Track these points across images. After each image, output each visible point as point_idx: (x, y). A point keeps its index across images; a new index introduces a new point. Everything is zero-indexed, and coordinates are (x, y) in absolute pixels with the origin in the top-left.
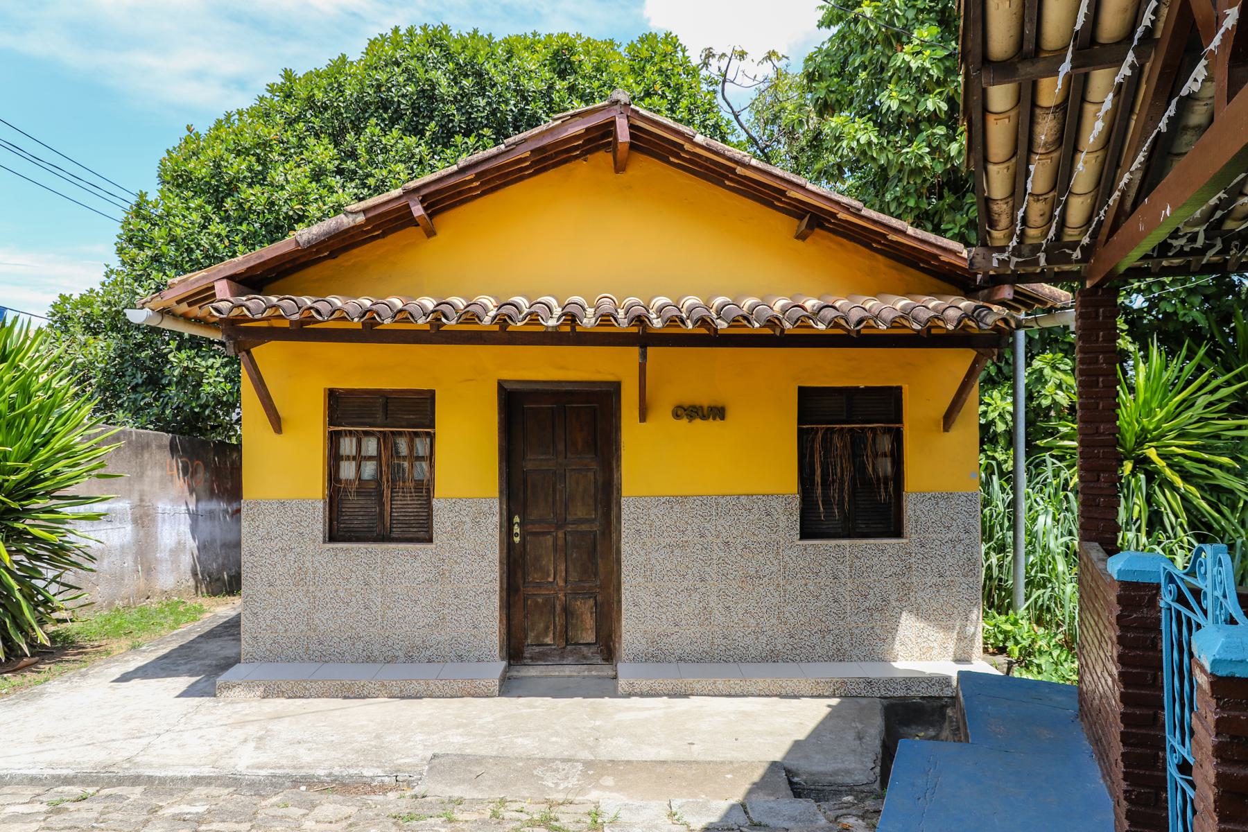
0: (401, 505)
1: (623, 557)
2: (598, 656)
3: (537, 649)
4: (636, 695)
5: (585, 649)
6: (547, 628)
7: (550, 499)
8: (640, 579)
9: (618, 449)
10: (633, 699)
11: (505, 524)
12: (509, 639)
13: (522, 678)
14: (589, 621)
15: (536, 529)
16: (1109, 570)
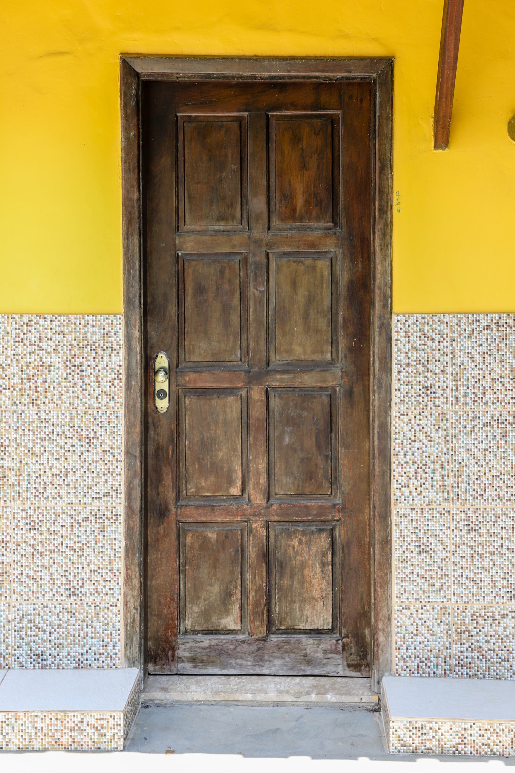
1: (395, 445)
2: (338, 659)
3: (206, 641)
4: (428, 753)
5: (309, 643)
6: (227, 595)
7: (235, 319)
8: (432, 495)
9: (386, 209)
10: (421, 762)
11: (138, 371)
12: (145, 620)
13: (173, 705)
14: (318, 582)
15: (206, 381)
16: (167, 405)
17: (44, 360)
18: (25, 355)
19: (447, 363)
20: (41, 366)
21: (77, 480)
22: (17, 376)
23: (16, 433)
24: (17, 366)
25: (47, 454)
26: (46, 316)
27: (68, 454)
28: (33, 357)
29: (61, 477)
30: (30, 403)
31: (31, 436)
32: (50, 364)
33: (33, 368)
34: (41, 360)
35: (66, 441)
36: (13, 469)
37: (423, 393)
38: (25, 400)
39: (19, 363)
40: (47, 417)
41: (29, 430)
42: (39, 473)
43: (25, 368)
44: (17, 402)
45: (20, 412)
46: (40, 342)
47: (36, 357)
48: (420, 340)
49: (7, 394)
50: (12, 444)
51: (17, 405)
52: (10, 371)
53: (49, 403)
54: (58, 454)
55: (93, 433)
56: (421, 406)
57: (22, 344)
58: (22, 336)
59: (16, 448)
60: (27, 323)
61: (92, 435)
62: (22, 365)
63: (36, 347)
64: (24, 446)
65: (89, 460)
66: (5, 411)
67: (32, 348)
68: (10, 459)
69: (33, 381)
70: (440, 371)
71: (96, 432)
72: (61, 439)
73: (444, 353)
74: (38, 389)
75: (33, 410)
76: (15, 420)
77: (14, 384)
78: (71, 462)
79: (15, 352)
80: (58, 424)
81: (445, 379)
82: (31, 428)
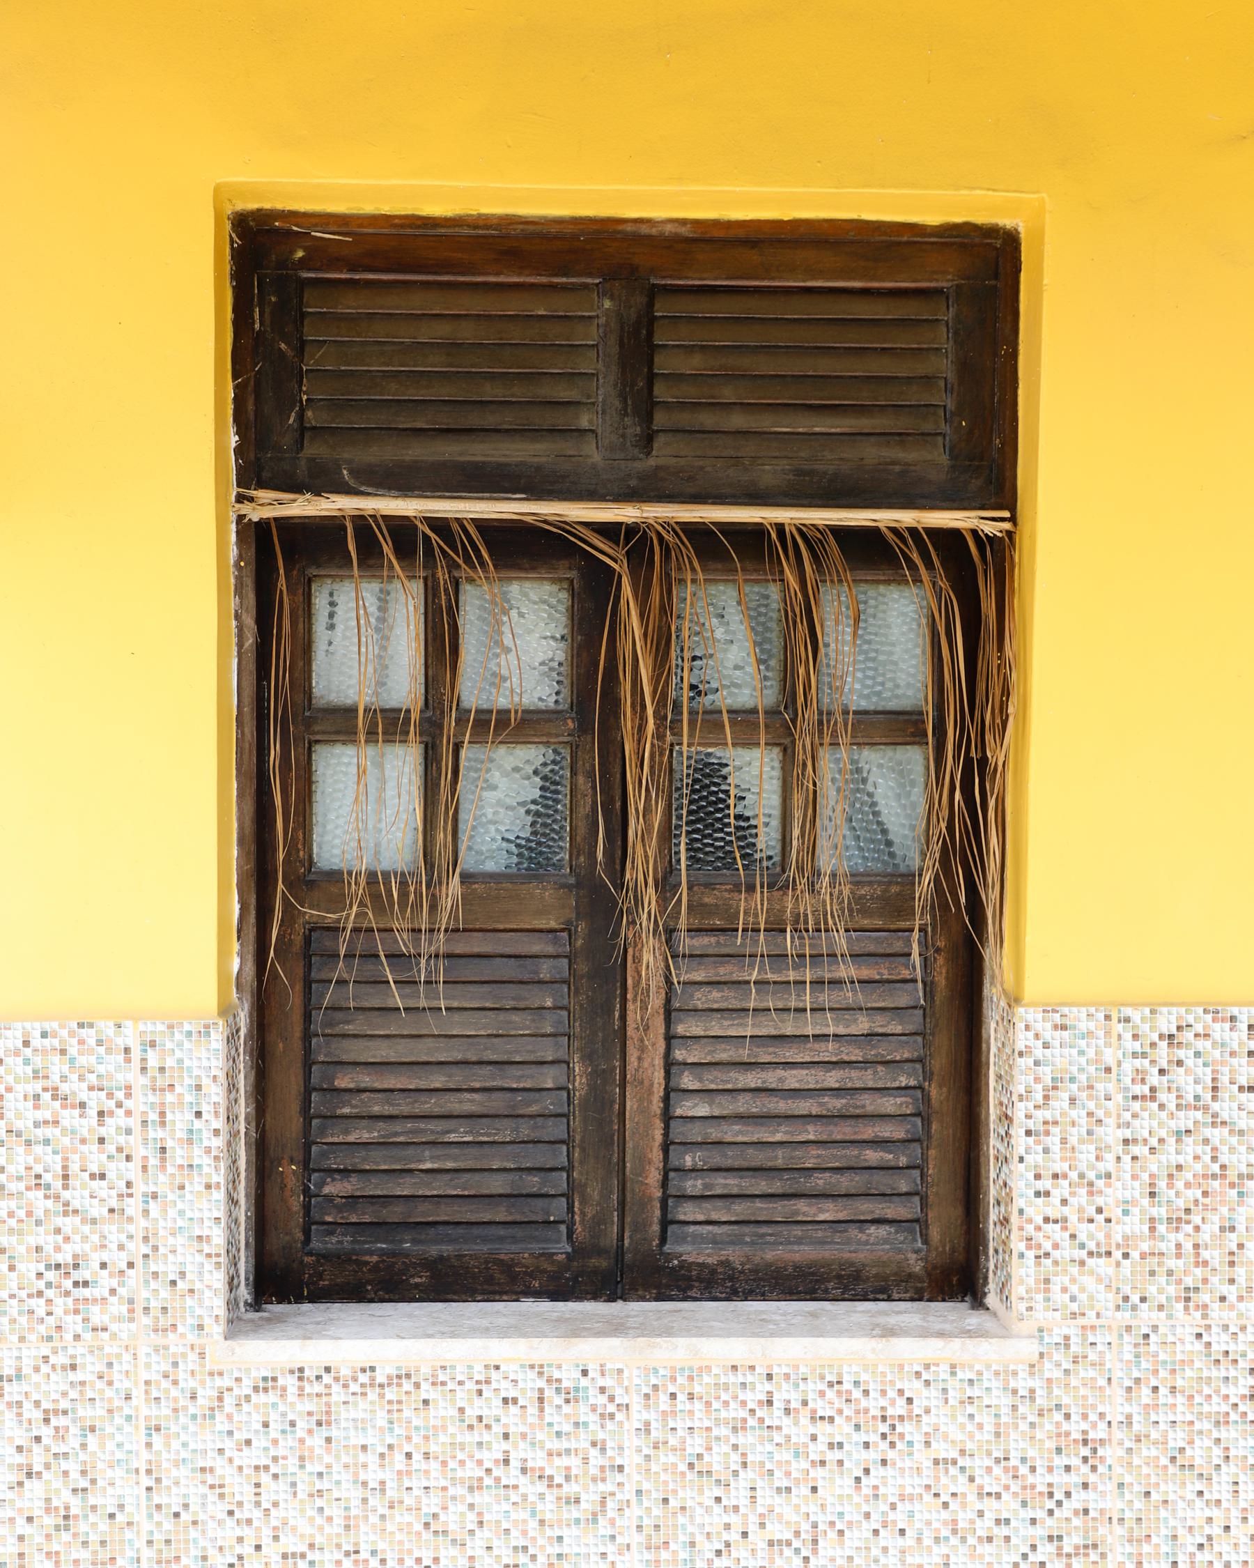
0: (758, 1046)
17: (1224, 1159)
18: (1161, 1141)
19: (129, 1185)
20: (1214, 1176)
21: (850, 1559)
22: (1135, 1211)
23: (1129, 1400)
24: (1134, 1177)
25: (1233, 1469)
26: (1235, 1011)
27: (819, 1472)
28: (1190, 1150)
29: (797, 1551)
30: (1178, 1299)
31: (698, 1415)
32: (1244, 1170)
33: (1188, 1185)
34: (1214, 1159)
35: (812, 1430)
36: (1121, 1520)
37: (49, 1285)
38: (1161, 1291)
39: (1143, 1169)
40: (1232, 1348)
41: (1173, 1390)
42: (1207, 1531)
43: (1162, 1184)
44: (1135, 1299)
45: (1145, 1331)
46: (1214, 1098)
47: (1199, 1149)
48: (36, 1107)
49: (1101, 1271)
50: (1118, 1434)
51: (1134, 1308)
52: (1111, 1197)
53: (1240, 1299)
54: (788, 1474)
55: (901, 1402)
56: (42, 1329)
57: (1155, 1106)
58: (1154, 1079)
59: (648, 1457)
60: (1171, 1036)
61: (900, 1408)
62: (1152, 1176)
63: (1199, 1115)
64: (1155, 1443)
65: (890, 1492)
66: (1093, 1328)
67: (1185, 1120)
68: (1111, 1487)
69: (1189, 1229)
70: (105, 1211)
71: (910, 1401)
72: (796, 1423)
73: (120, 1150)
74: (1205, 1254)
75: (1187, 1323)
76: (1128, 1356)
77: (1126, 1238)
78: (830, 1500)
79: (1128, 1134)
80: (787, 1376)
81: (123, 1237)
82: (1179, 1383)
